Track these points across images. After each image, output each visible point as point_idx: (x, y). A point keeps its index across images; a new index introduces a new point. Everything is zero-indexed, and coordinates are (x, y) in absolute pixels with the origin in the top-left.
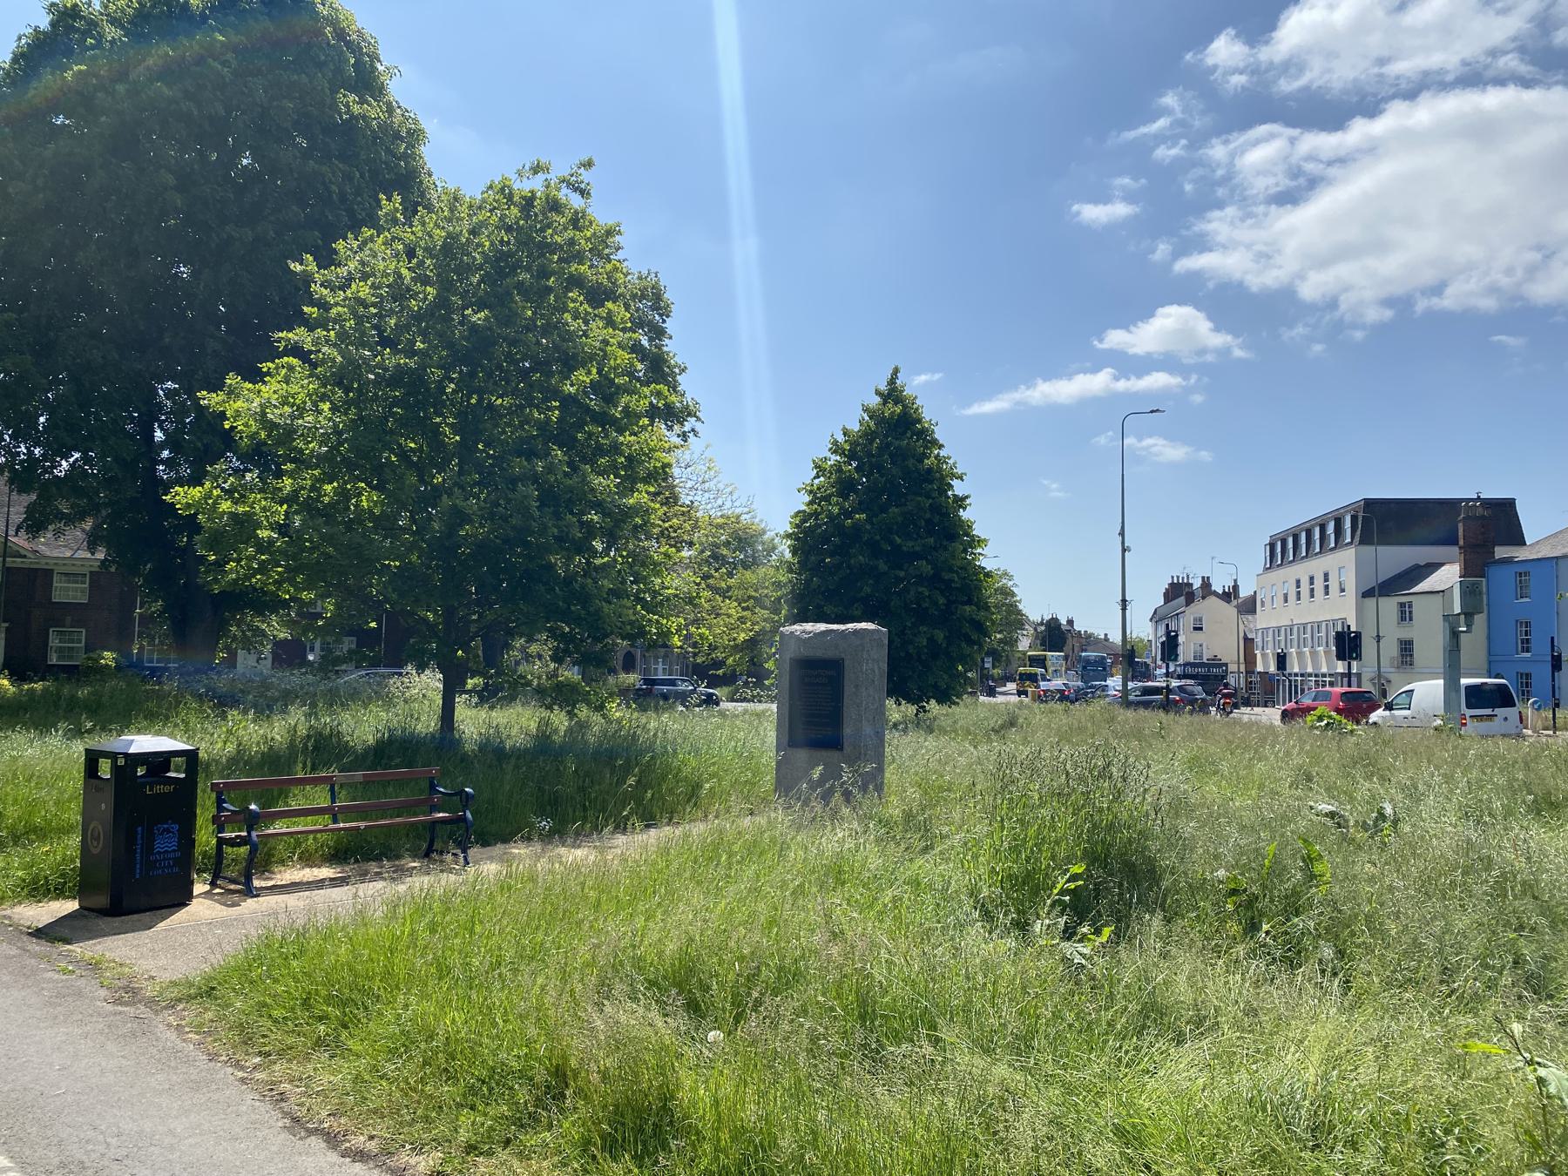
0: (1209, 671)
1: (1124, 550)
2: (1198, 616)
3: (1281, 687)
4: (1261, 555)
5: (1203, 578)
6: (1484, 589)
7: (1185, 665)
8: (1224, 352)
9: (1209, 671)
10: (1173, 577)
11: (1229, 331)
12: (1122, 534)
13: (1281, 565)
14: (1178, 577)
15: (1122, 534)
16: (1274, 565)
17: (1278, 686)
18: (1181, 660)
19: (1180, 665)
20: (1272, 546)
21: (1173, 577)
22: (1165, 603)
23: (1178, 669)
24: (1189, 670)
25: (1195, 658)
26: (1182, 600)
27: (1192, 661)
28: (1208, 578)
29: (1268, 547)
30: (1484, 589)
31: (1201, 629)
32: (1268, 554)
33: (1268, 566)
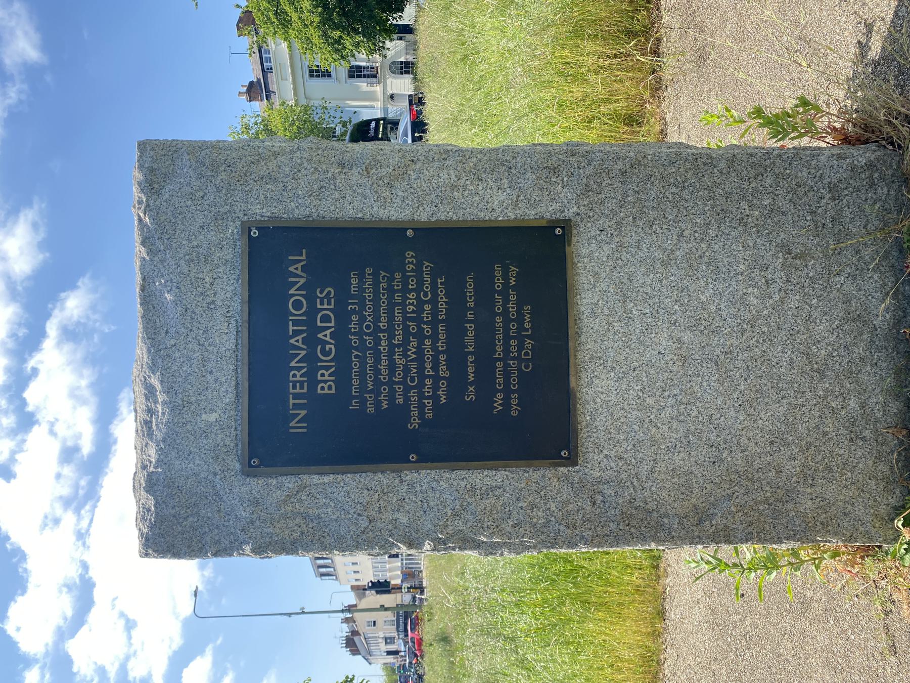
0: (401, 616)
1: (303, 613)
2: (366, 624)
3: (410, 566)
4: (328, 582)
5: (342, 622)
6: (275, 80)
7: (398, 631)
8: (217, 652)
9: (401, 616)
10: (342, 647)
11: (206, 645)
12: (290, 615)
13: (334, 568)
14: (342, 644)
15: (290, 615)
16: (334, 573)
17: (409, 568)
18: (396, 635)
19: (398, 635)
20: (322, 575)
21: (342, 647)
22: (360, 654)
23: (401, 636)
24: (402, 628)
25: (393, 625)
26: (356, 639)
27: (395, 627)
28: (342, 619)
29: (323, 578)
30: (275, 80)
31: (375, 622)
32: (327, 578)
33: (334, 577)
